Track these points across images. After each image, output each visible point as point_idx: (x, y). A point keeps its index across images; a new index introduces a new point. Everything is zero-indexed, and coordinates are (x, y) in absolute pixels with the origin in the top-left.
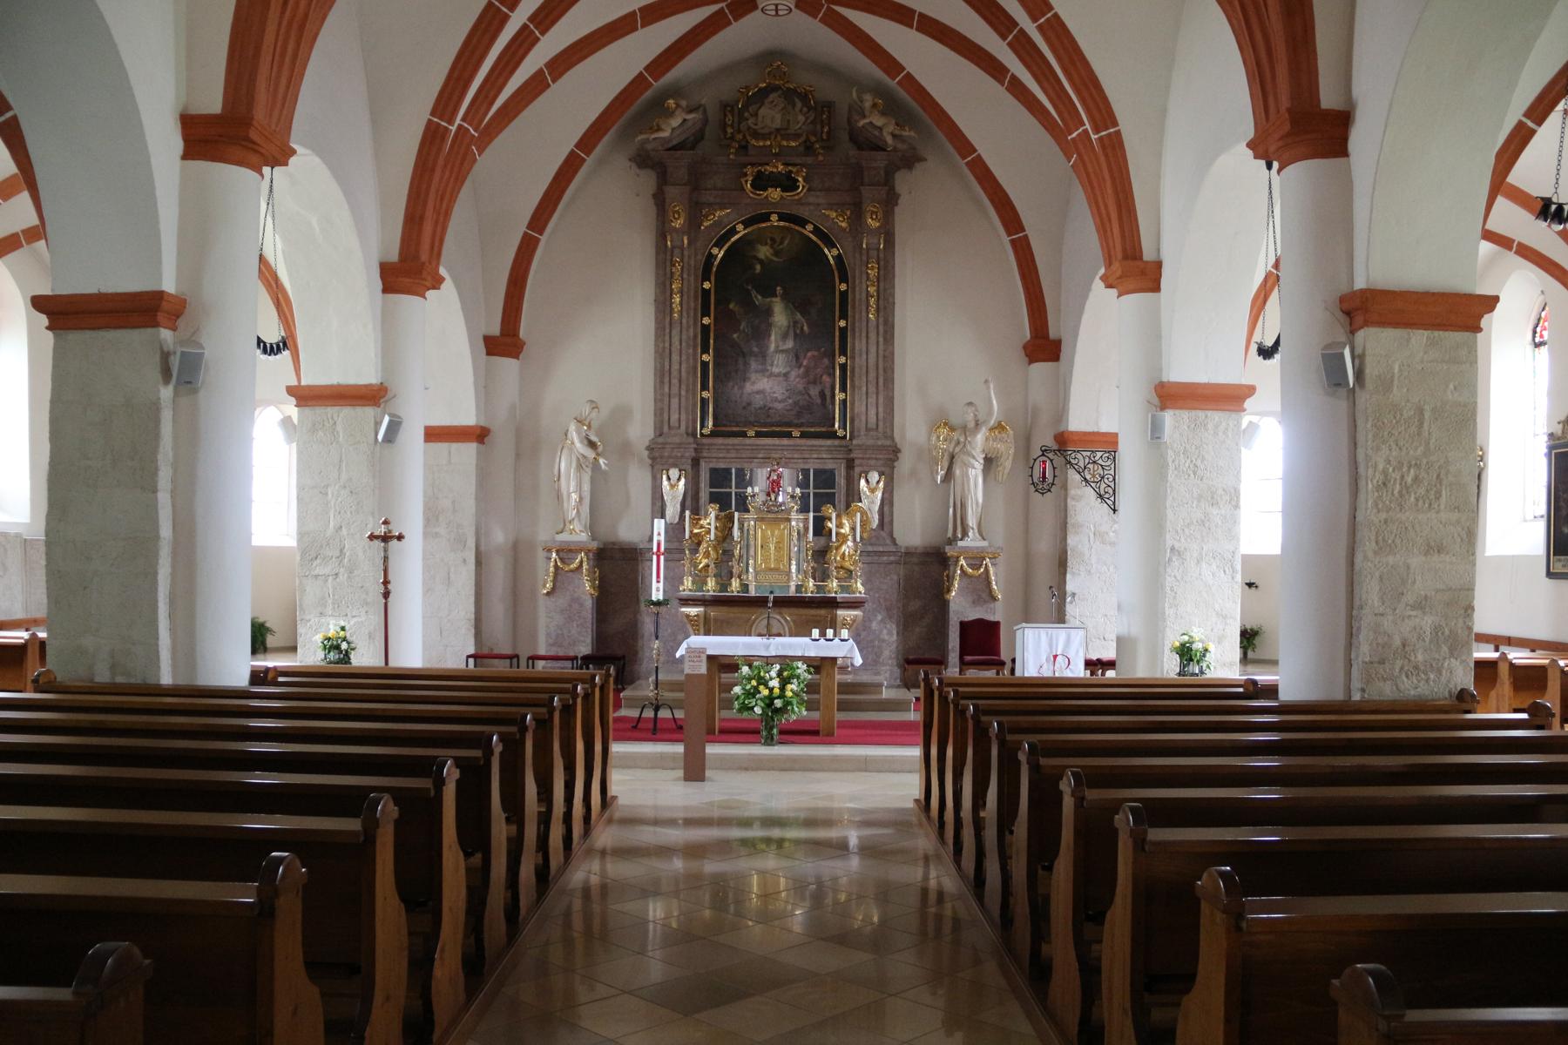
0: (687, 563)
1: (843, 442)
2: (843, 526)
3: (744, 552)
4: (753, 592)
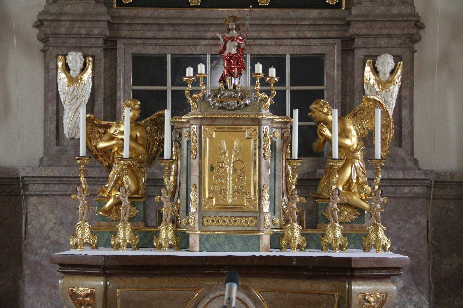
0: (82, 202)
1: (337, 13)
2: (341, 134)
3: (182, 179)
4: (195, 251)
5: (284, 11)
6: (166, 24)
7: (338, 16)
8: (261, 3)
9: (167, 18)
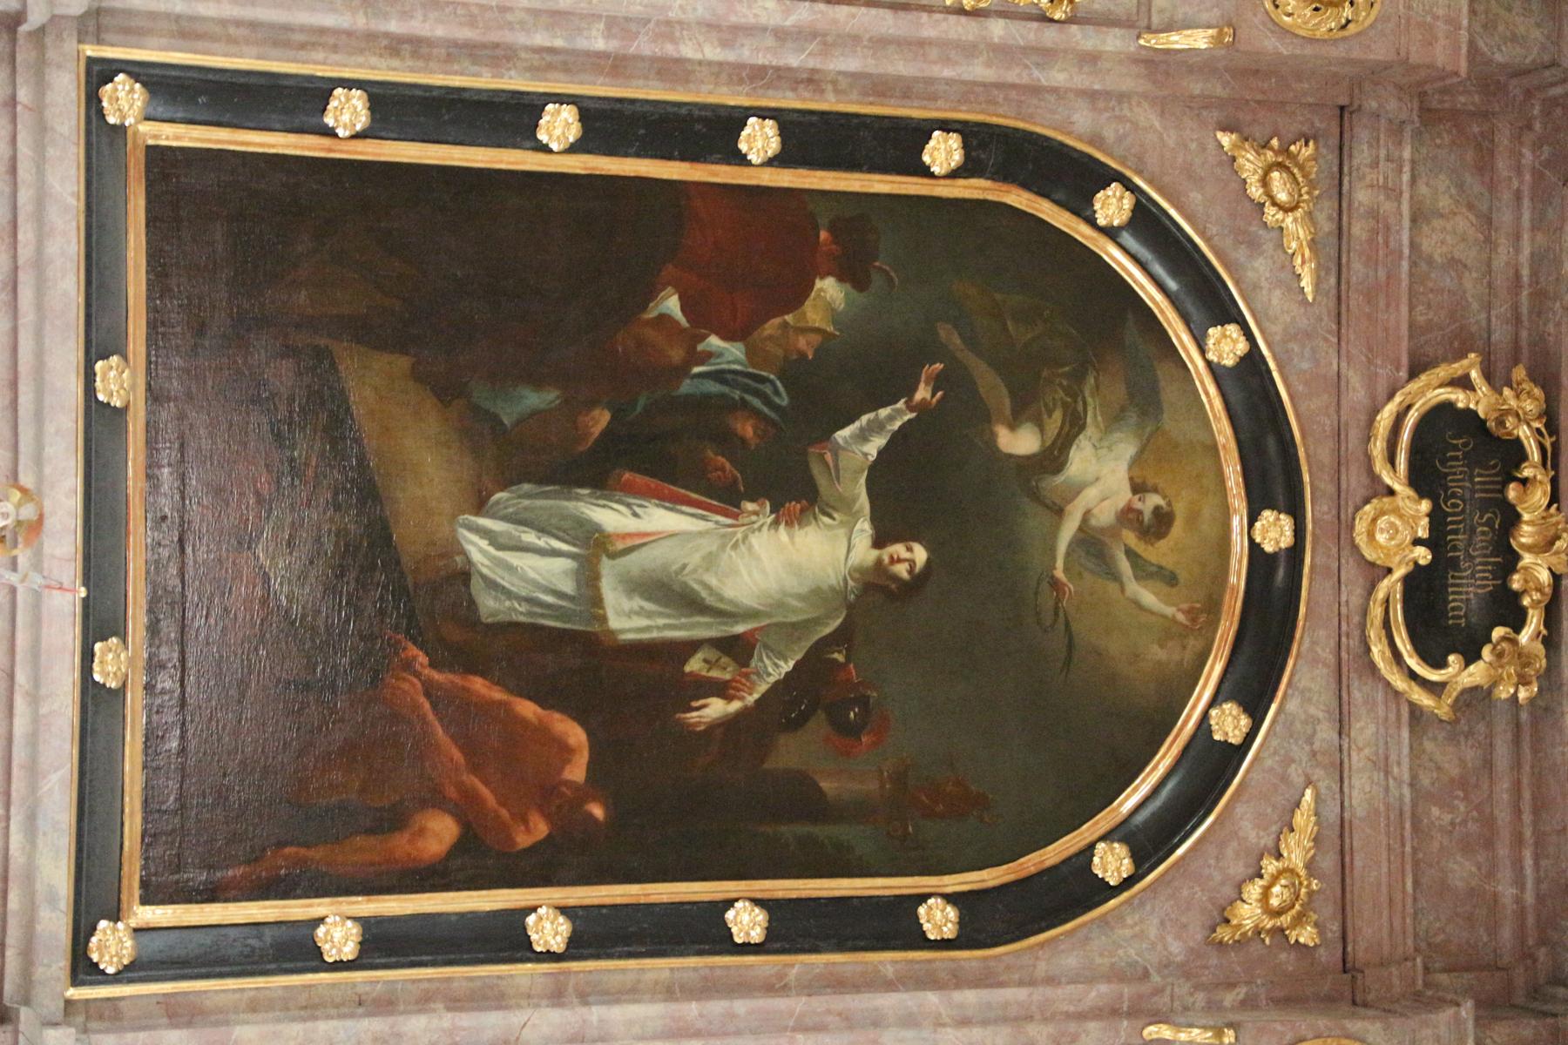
1: (55, 964)
5: (67, 746)
6: (15, 257)
7: (39, 973)
8: (103, 654)
9: (39, 263)
